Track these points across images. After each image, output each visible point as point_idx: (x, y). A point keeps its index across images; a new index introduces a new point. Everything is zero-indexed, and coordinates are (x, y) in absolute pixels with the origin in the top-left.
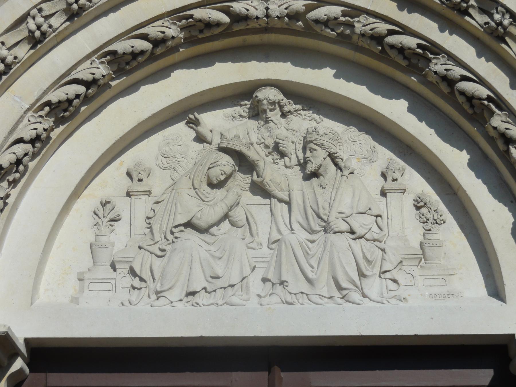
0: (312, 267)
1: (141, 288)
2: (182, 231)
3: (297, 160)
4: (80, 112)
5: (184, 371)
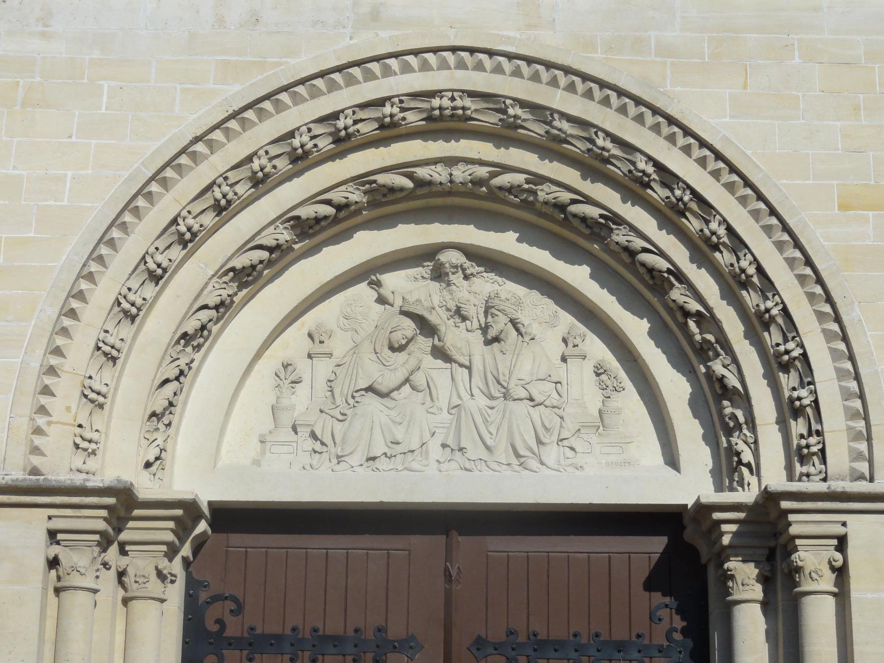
0: (491, 434)
1: (322, 452)
2: (364, 395)
3: (478, 324)
4: (263, 274)
5: (364, 534)
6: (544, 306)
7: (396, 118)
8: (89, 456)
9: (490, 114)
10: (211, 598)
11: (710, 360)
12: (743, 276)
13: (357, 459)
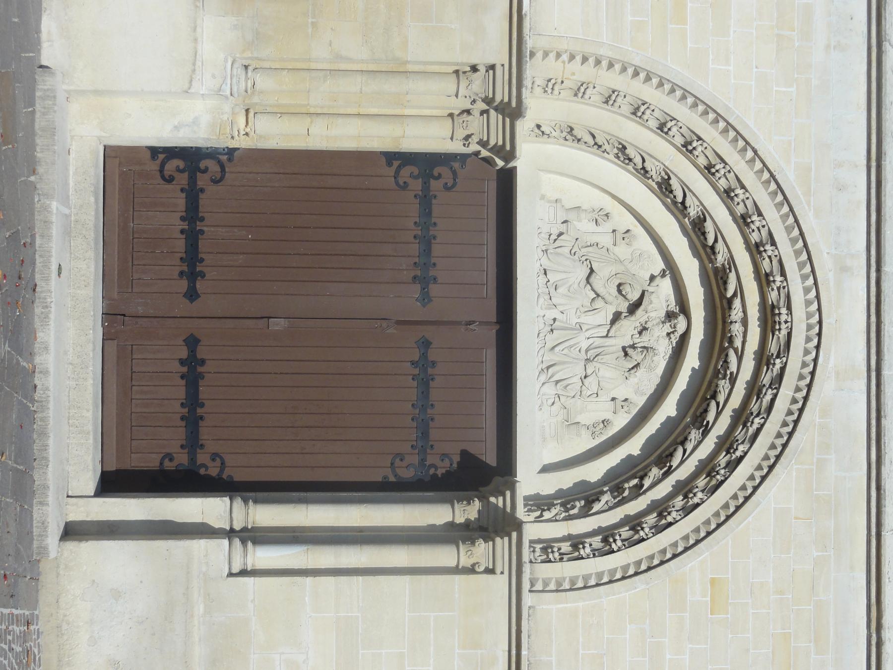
0: (562, 350)
6: (649, 387)
8: (543, 89)
9: (777, 347)
10: (455, 170)
11: (611, 493)
12: (666, 514)
13: (545, 262)
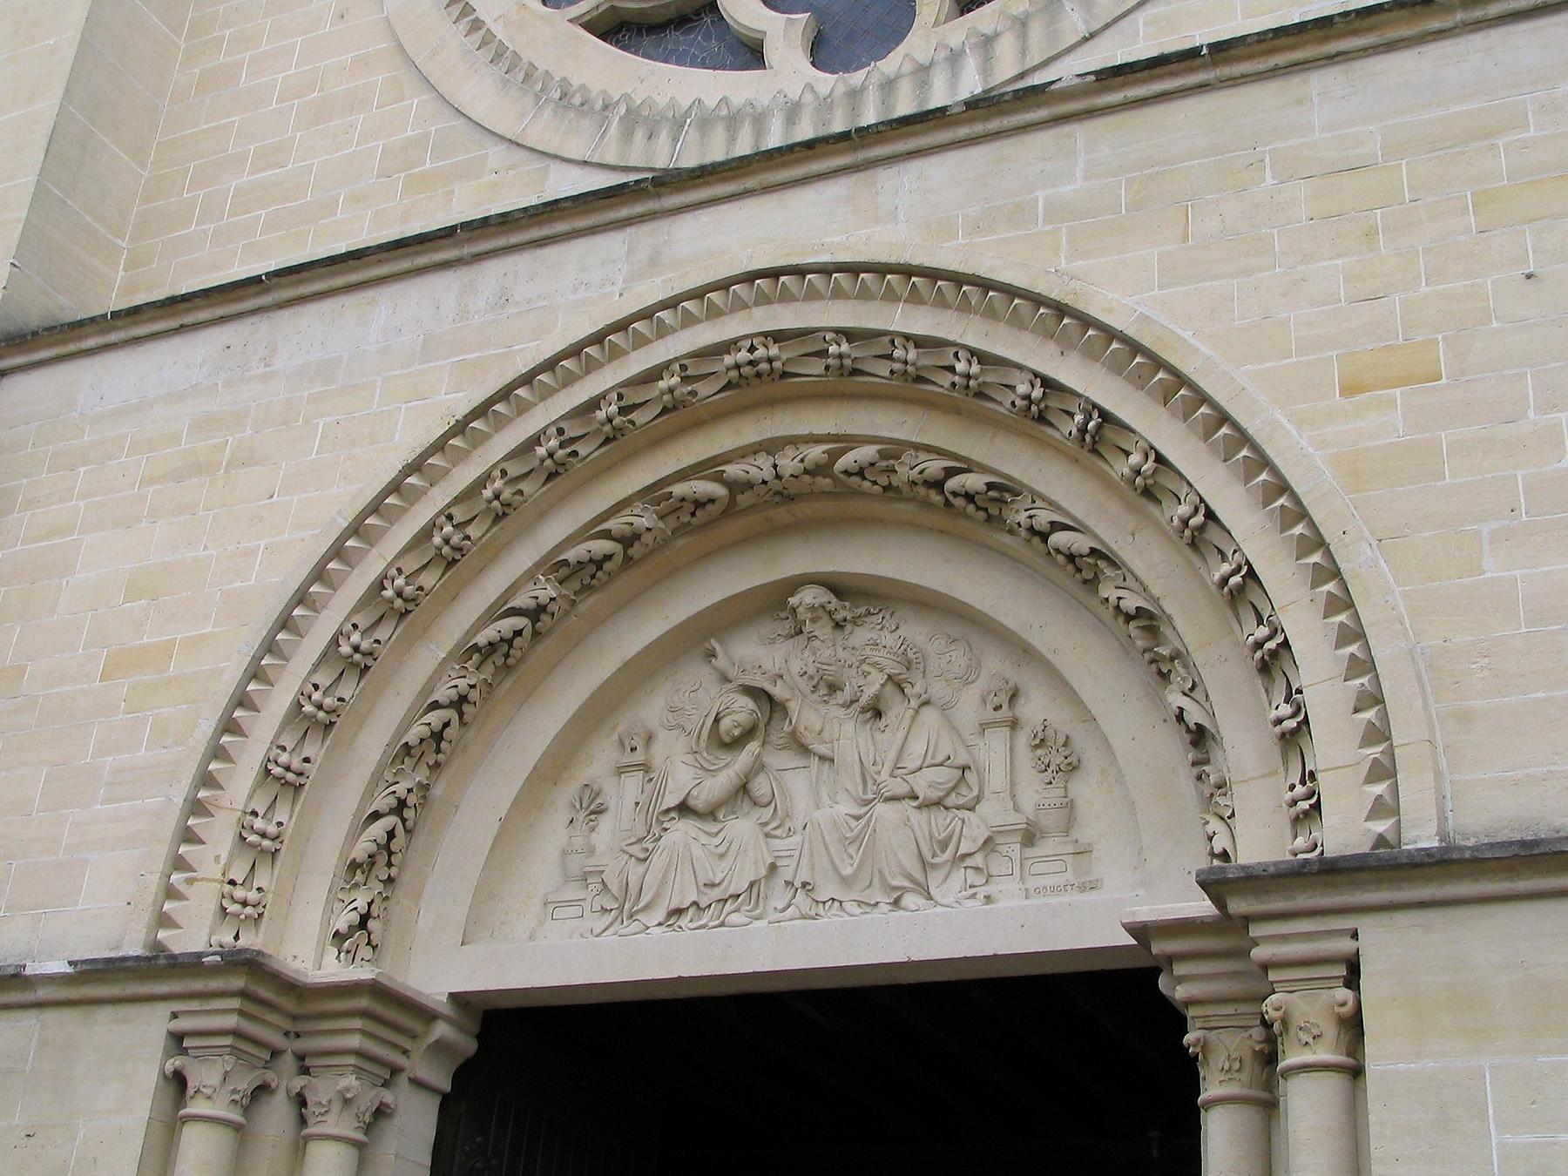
7: (677, 393)
